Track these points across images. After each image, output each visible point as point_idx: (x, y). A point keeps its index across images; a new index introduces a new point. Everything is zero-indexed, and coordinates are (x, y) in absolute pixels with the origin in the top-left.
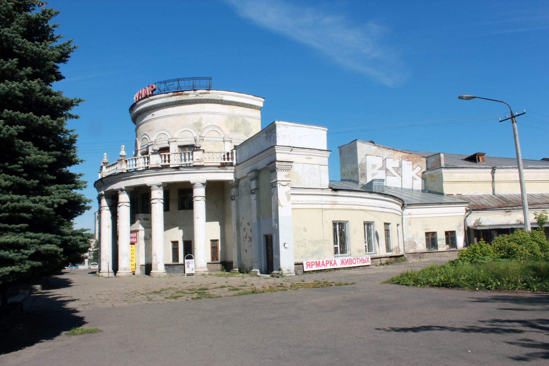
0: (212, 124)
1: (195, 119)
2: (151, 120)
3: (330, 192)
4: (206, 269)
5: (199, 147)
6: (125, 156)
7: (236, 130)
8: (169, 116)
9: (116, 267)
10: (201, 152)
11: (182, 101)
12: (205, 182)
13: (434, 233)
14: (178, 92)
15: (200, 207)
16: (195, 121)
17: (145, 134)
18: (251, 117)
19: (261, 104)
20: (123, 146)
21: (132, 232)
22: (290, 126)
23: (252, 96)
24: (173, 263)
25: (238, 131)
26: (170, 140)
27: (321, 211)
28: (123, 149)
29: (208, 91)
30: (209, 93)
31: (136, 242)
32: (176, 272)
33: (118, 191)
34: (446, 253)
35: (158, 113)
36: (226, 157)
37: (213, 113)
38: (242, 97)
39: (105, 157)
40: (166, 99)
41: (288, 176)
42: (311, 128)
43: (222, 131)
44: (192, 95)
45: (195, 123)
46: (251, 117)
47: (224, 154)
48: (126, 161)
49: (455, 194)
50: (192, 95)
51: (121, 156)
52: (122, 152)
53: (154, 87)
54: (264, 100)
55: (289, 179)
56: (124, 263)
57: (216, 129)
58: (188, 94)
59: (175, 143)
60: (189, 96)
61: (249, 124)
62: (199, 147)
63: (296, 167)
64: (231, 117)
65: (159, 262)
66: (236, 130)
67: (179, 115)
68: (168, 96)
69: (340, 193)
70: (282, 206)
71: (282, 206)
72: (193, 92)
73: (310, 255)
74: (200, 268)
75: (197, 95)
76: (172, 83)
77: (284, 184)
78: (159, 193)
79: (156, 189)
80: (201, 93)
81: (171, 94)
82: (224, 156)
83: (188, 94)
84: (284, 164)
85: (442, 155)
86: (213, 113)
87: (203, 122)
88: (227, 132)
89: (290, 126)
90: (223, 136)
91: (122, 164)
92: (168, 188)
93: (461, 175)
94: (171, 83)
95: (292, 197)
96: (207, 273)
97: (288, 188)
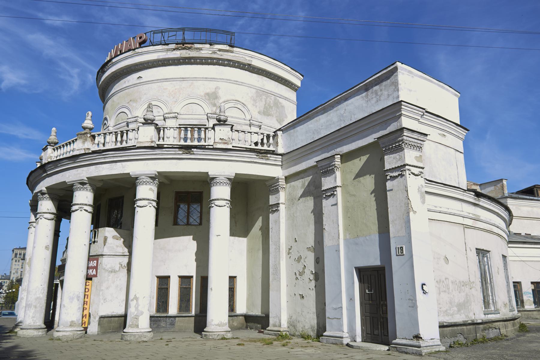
0: (234, 98)
1: (210, 87)
2: (135, 85)
3: (470, 197)
4: (227, 328)
5: (225, 121)
6: (91, 129)
7: (266, 113)
8: (166, 80)
9: (49, 323)
10: (228, 129)
11: (190, 58)
12: (232, 175)
13: (519, 283)
14: (183, 44)
15: (220, 217)
16: (208, 91)
17: (123, 107)
18: (286, 99)
19: (298, 83)
20: (90, 113)
21: (91, 258)
22: (417, 75)
23: (289, 69)
24: (158, 315)
25: (269, 115)
26: (166, 115)
27: (462, 227)
28: (89, 117)
29: (231, 49)
30: (232, 52)
31: (96, 276)
32: (162, 330)
33: (72, 185)
34: (535, 313)
35: (147, 74)
36: (265, 141)
37: (236, 82)
38: (276, 66)
39: (53, 133)
40: (164, 53)
41: (419, 158)
42: (442, 87)
43: (249, 111)
44: (206, 51)
45: (207, 94)
46: (286, 99)
47: (262, 137)
48: (94, 137)
49: (523, 234)
50: (206, 51)
51: (85, 128)
52: (86, 122)
53: (144, 37)
54: (302, 77)
55: (421, 165)
56: (68, 313)
57: (239, 106)
58: (200, 49)
59: (174, 120)
60: (202, 52)
61: (283, 107)
62: (225, 121)
63: (427, 146)
64: (262, 92)
65: (142, 313)
66: (266, 113)
67: (183, 79)
68: (168, 50)
69: (483, 202)
70: (415, 212)
71: (415, 212)
72: (208, 46)
73: (455, 309)
74: (218, 325)
75: (214, 53)
76: (174, 33)
77: (416, 173)
78: (151, 189)
79: (146, 183)
80: (220, 50)
81: (173, 46)
82: (262, 140)
83: (200, 49)
84: (415, 136)
85: (505, 182)
86: (236, 82)
87: (221, 93)
88: (255, 113)
89: (417, 75)
90: (248, 117)
91: (86, 140)
92: (166, 183)
93: (530, 209)
94: (171, 34)
95: (427, 197)
96: (229, 335)
97: (420, 181)
